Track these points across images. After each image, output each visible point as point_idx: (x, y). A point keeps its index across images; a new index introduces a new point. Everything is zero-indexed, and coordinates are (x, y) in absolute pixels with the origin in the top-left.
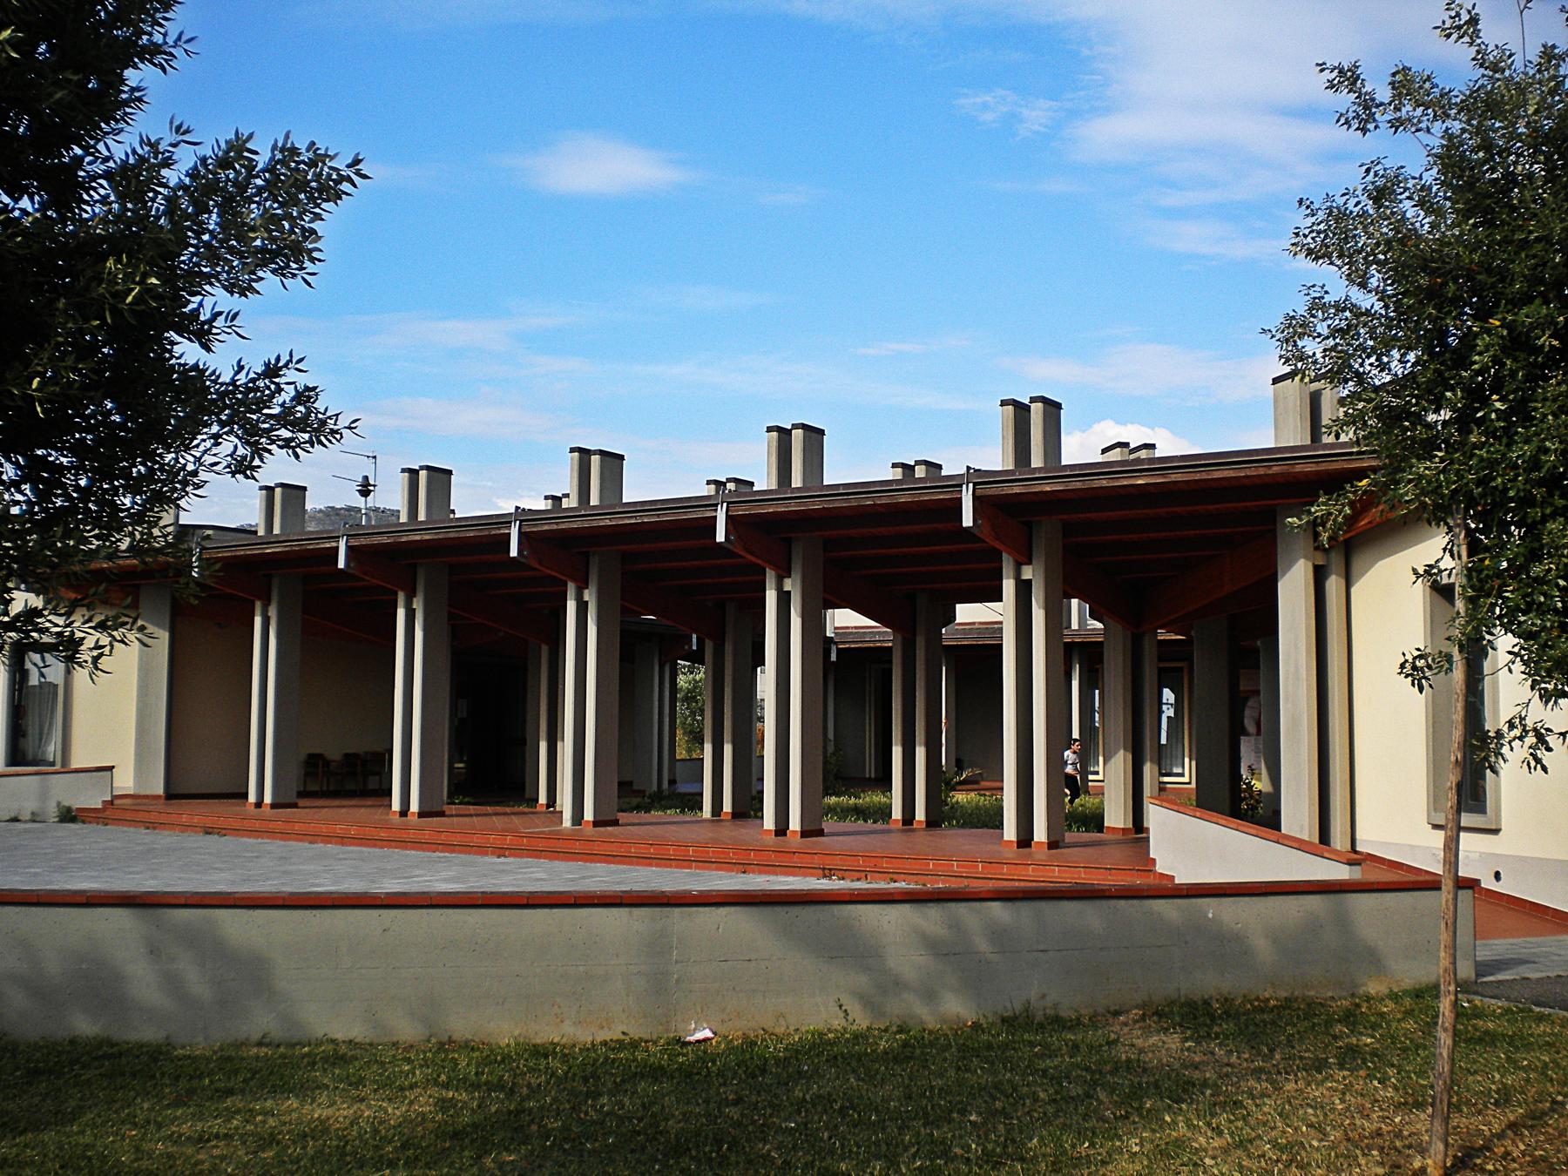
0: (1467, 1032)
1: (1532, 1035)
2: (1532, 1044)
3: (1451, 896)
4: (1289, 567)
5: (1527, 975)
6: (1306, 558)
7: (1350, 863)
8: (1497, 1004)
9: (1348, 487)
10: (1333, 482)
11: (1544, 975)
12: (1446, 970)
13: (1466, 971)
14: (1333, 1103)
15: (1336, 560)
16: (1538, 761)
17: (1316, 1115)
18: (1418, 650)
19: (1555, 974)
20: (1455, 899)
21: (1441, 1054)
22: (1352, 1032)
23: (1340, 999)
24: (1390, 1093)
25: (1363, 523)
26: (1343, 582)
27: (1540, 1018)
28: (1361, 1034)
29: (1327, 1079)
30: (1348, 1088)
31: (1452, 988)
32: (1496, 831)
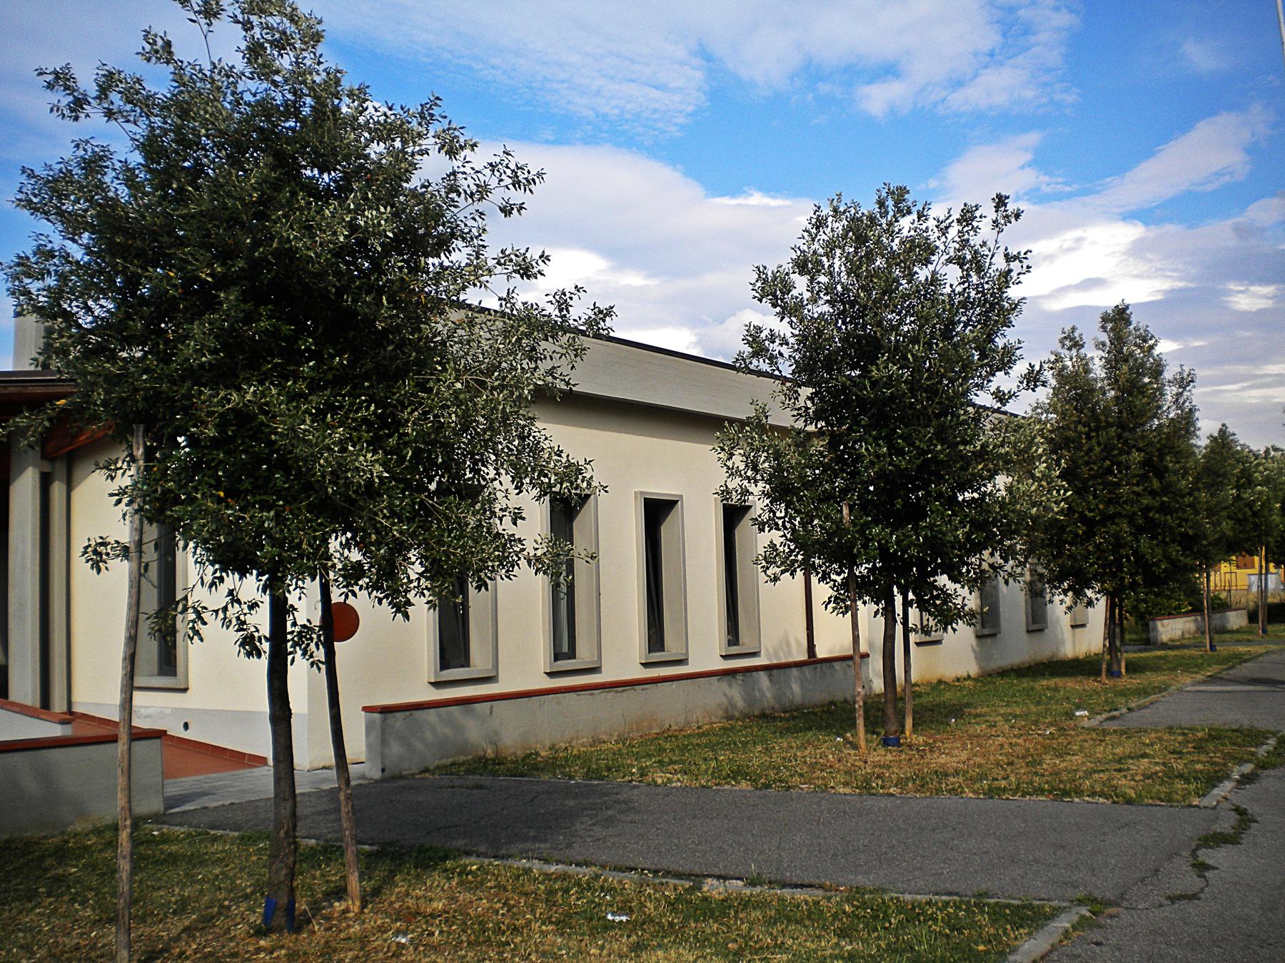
0: (154, 856)
1: (206, 853)
2: (206, 860)
3: (125, 747)
4: (21, 472)
5: (207, 805)
6: (33, 466)
7: (63, 722)
8: (181, 830)
9: (48, 405)
10: (36, 403)
11: (220, 803)
12: (122, 809)
13: (153, 804)
14: (40, 926)
15: (60, 469)
16: (197, 633)
17: (25, 938)
18: (101, 538)
19: (229, 802)
20: (130, 749)
21: (121, 877)
22: (59, 864)
23: (51, 837)
24: (89, 912)
25: (84, 437)
26: (64, 487)
27: (215, 839)
28: (67, 865)
29: (36, 906)
30: (54, 912)
31: (128, 822)
32: (185, 690)
